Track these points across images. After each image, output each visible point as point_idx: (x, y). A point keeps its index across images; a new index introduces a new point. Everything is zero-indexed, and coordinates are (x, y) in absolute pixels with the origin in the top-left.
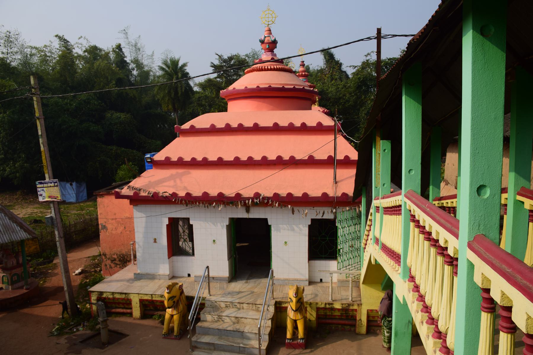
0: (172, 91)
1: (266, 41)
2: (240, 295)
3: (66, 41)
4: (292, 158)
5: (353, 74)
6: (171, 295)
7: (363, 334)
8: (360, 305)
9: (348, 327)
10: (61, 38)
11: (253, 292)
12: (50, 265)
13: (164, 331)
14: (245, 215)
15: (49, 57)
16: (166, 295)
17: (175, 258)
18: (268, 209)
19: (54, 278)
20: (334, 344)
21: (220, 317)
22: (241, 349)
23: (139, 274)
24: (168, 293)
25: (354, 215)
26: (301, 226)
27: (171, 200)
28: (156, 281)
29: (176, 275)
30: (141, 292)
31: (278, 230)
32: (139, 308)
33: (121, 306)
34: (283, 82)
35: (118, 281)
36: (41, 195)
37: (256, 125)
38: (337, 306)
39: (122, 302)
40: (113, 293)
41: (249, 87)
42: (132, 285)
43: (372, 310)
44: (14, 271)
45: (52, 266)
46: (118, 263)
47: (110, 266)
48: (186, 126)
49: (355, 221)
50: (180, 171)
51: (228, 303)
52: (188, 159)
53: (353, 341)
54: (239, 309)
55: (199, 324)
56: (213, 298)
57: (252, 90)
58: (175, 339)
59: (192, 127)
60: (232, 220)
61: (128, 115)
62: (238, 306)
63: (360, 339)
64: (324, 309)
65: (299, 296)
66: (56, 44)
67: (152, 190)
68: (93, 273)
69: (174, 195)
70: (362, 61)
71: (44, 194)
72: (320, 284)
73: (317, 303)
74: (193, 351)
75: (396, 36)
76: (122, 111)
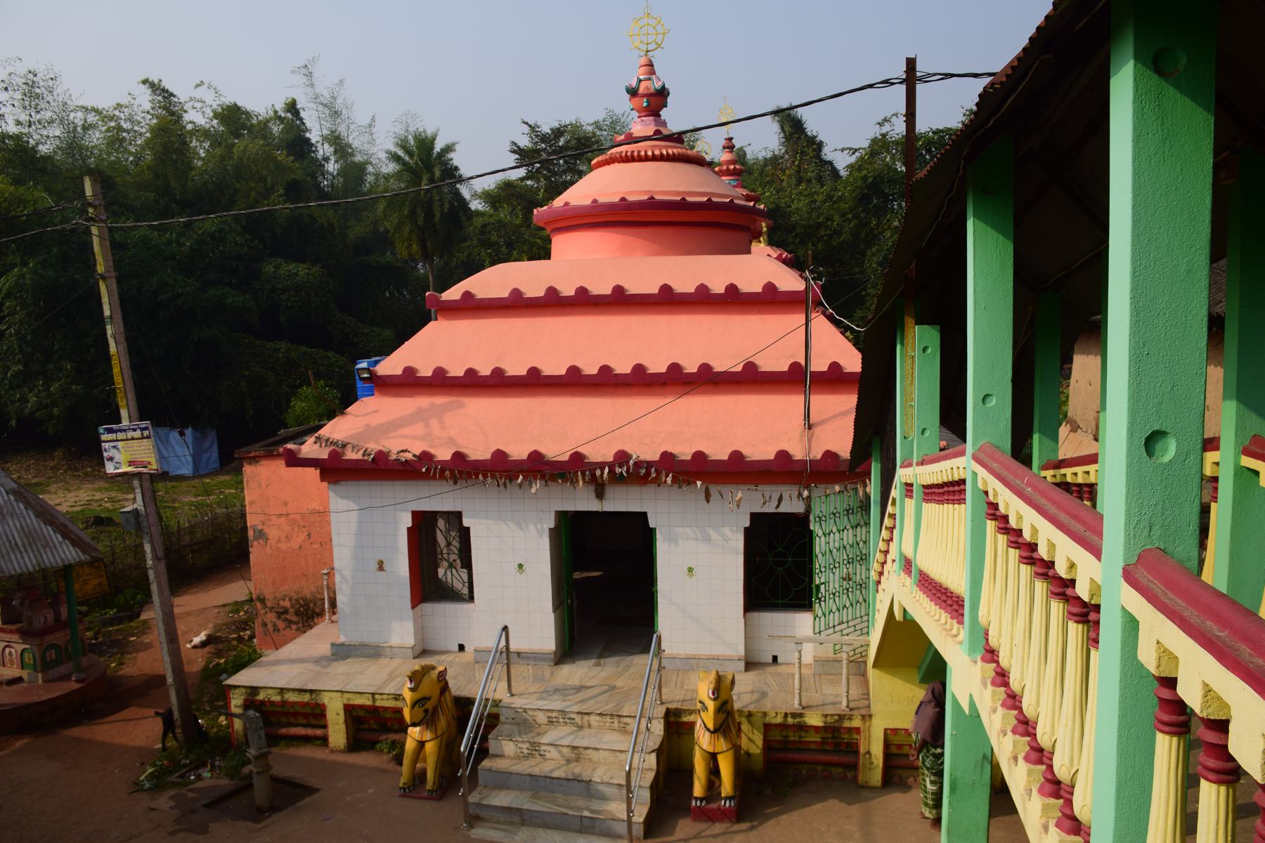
0: (419, 210)
1: (641, 90)
2: (581, 696)
3: (167, 94)
4: (705, 368)
5: (850, 166)
6: (418, 695)
7: (875, 788)
8: (867, 717)
9: (840, 770)
10: (155, 87)
11: (613, 688)
12: (133, 624)
13: (429, 785)
15: (128, 131)
16: (408, 696)
17: (428, 607)
18: (649, 490)
20: (806, 811)
21: (535, 746)
22: (586, 822)
23: (342, 644)
24: (411, 690)
25: (854, 503)
26: (726, 530)
27: (419, 469)
28: (384, 661)
29: (432, 648)
30: (348, 689)
31: (672, 540)
32: (343, 726)
33: (302, 720)
34: (681, 189)
35: (294, 661)
36: (111, 459)
37: (618, 290)
38: (814, 720)
39: (302, 710)
40: (282, 691)
41: (602, 200)
42: (328, 670)
43: (895, 731)
44: (49, 639)
45: (137, 628)
46: (294, 618)
47: (275, 625)
48: (453, 294)
49: (855, 519)
50: (440, 400)
51: (554, 714)
52: (457, 371)
53: (850, 804)
54: (581, 728)
55: (486, 763)
56: (518, 702)
57: (610, 207)
58: (430, 798)
60: (562, 516)
62: (578, 719)
63: (867, 800)
64: (783, 726)
65: (723, 697)
66: (145, 100)
67: (374, 447)
68: (235, 643)
69: (426, 457)
70: (872, 136)
71: (118, 457)
72: (772, 669)
73: (765, 714)
74: (471, 826)
75: (953, 75)
76: (301, 259)
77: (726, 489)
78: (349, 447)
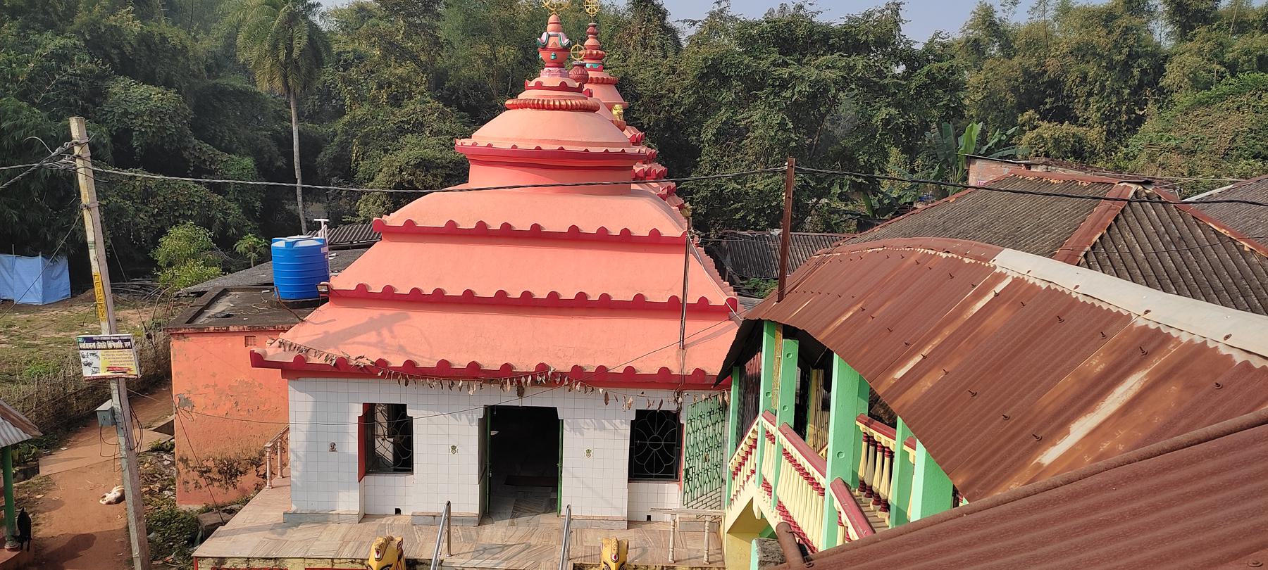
0: (281, 46)
1: (550, 45)
2: (505, 554)
4: (605, 297)
5: (690, 39)
6: (383, 564)
11: (529, 546)
12: (34, 480)
14: (516, 402)
17: (370, 479)
18: (559, 392)
19: (55, 514)
24: (378, 560)
25: (715, 407)
26: (617, 422)
27: (379, 371)
30: (309, 555)
35: (250, 530)
36: (89, 364)
37: (536, 227)
41: (521, 146)
42: (285, 537)
45: (40, 484)
46: (218, 476)
48: (396, 219)
50: (389, 312)
57: (527, 153)
59: (410, 223)
61: (171, 94)
67: (336, 353)
68: (147, 496)
69: (381, 364)
71: (96, 362)
72: (648, 526)
76: (149, 80)
77: (621, 392)
78: (312, 353)
